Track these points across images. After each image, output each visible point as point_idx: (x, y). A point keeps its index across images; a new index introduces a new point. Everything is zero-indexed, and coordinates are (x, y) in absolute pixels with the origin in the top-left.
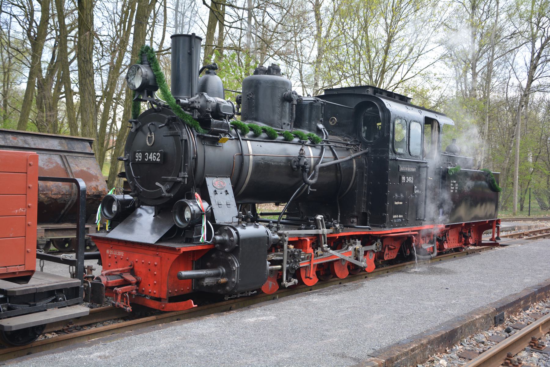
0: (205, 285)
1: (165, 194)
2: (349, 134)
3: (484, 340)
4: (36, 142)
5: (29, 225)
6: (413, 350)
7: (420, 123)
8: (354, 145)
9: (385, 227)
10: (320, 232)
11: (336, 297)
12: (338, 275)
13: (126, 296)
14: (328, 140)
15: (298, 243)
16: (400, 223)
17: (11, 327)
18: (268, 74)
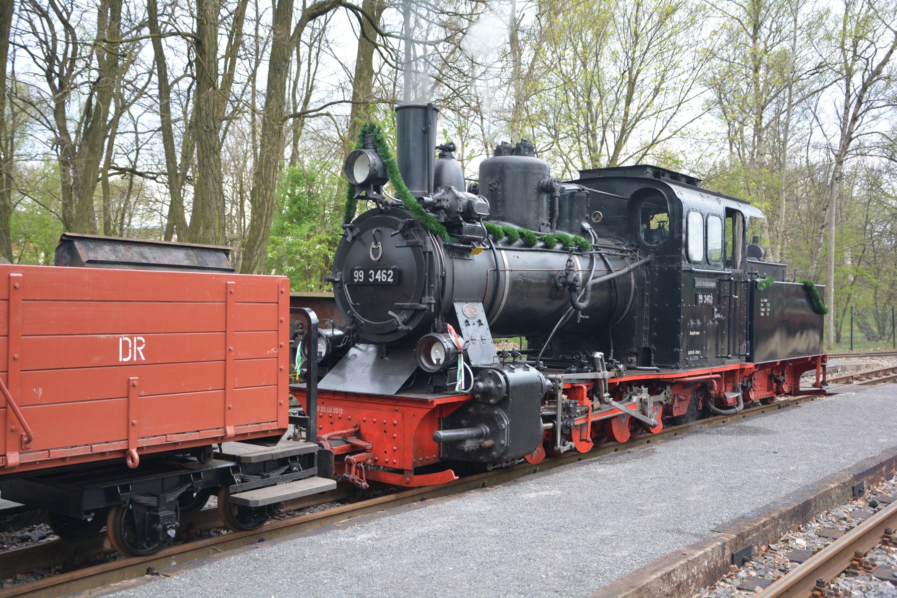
0: (466, 449)
1: (402, 327)
2: (621, 235)
3: (845, 515)
4: (156, 254)
5: (281, 370)
6: (764, 525)
7: (719, 216)
8: (631, 252)
9: (678, 368)
10: (600, 375)
11: (628, 466)
12: (618, 438)
13: (361, 468)
14: (597, 245)
15: (572, 391)
16: (698, 361)
17: (257, 502)
18: (516, 155)
